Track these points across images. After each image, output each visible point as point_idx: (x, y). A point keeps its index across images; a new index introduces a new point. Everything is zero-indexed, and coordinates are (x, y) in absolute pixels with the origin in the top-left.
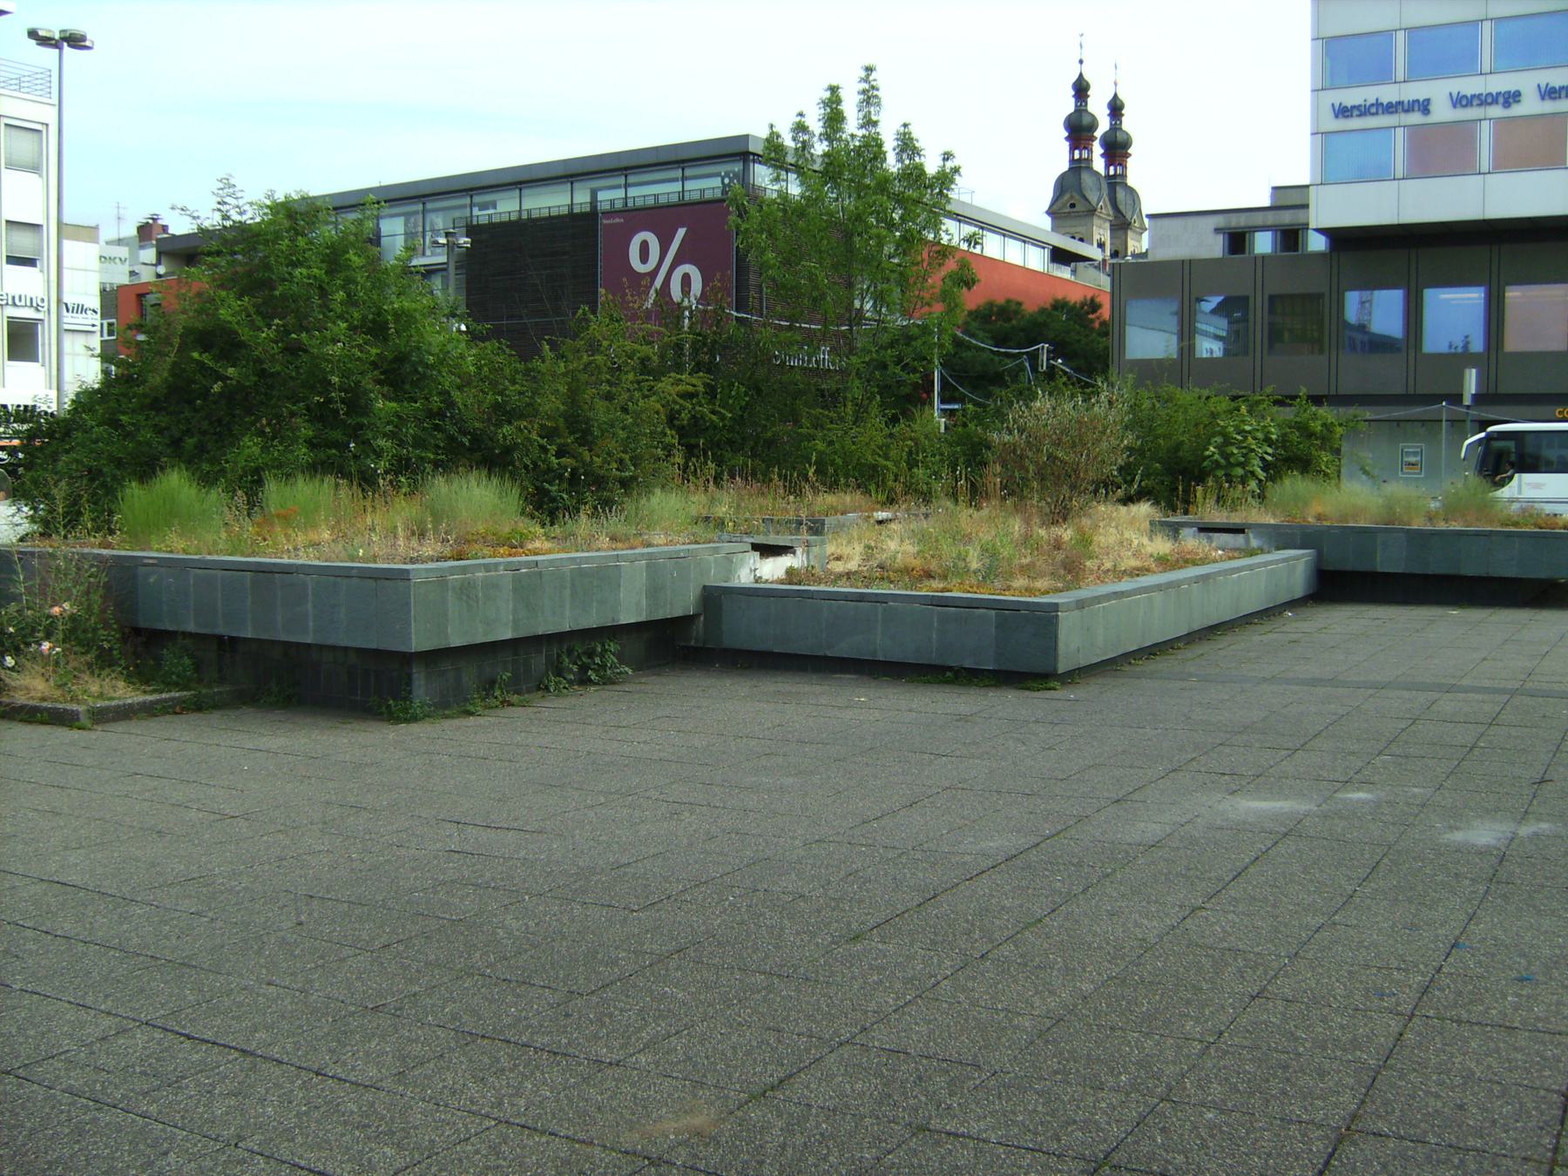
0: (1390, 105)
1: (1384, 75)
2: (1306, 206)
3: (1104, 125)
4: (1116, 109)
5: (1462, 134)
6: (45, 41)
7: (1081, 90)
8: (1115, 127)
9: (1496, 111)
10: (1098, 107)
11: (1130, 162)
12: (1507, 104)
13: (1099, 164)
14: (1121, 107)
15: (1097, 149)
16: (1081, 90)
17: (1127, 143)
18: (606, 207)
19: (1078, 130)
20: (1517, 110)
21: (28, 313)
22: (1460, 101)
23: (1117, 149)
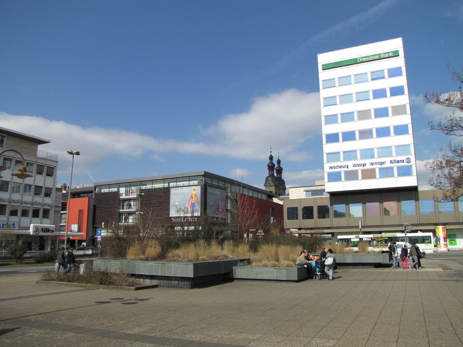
0: (340, 166)
1: (339, 160)
2: (324, 185)
3: (276, 166)
4: (279, 162)
5: (356, 172)
6: (71, 153)
7: (271, 158)
8: (279, 166)
9: (362, 168)
10: (275, 162)
11: (282, 174)
12: (363, 166)
13: (275, 175)
14: (273, 157)
15: (275, 171)
16: (271, 158)
17: (282, 169)
18: (172, 186)
19: (271, 167)
20: (365, 168)
21: (48, 208)
22: (354, 165)
23: (280, 171)
